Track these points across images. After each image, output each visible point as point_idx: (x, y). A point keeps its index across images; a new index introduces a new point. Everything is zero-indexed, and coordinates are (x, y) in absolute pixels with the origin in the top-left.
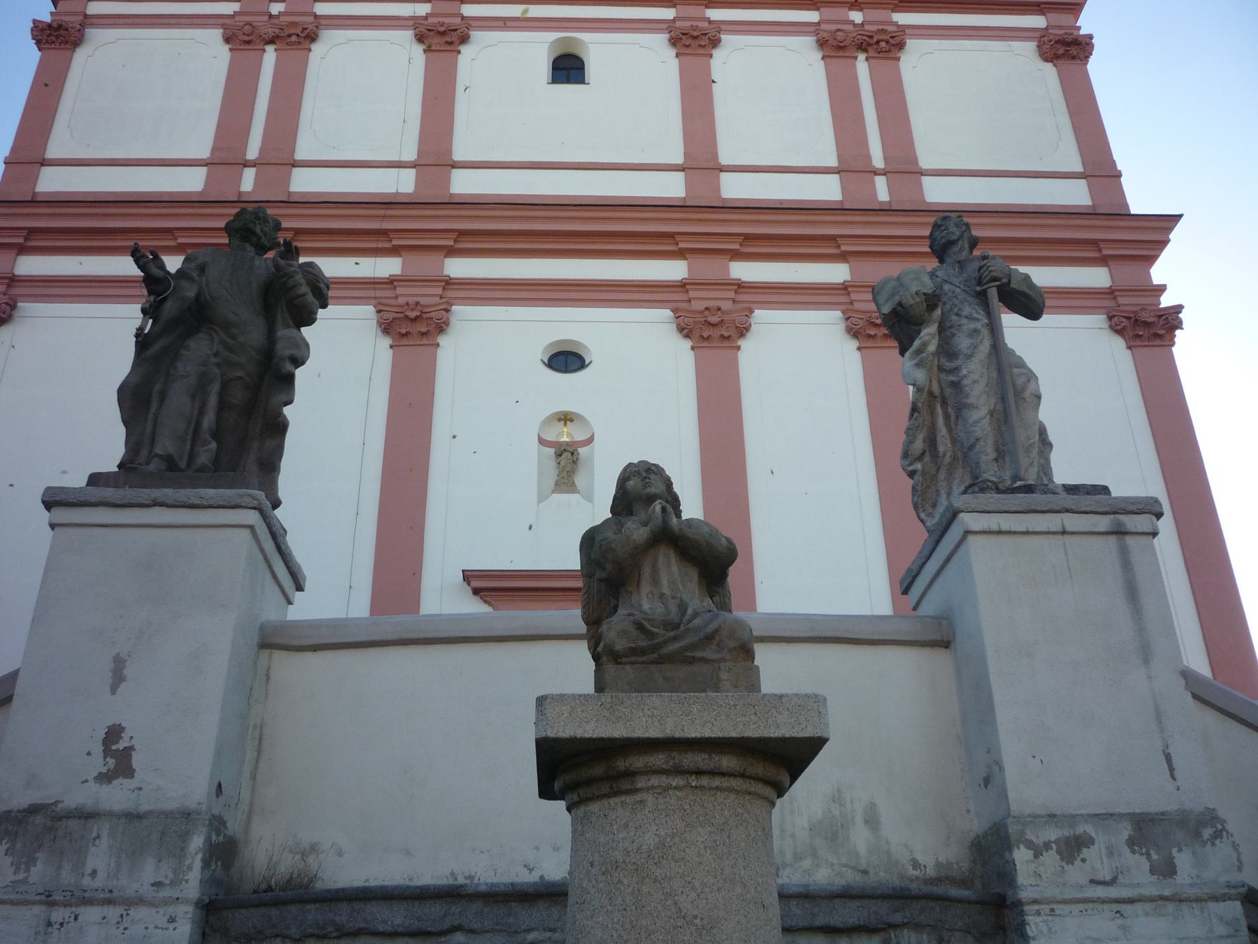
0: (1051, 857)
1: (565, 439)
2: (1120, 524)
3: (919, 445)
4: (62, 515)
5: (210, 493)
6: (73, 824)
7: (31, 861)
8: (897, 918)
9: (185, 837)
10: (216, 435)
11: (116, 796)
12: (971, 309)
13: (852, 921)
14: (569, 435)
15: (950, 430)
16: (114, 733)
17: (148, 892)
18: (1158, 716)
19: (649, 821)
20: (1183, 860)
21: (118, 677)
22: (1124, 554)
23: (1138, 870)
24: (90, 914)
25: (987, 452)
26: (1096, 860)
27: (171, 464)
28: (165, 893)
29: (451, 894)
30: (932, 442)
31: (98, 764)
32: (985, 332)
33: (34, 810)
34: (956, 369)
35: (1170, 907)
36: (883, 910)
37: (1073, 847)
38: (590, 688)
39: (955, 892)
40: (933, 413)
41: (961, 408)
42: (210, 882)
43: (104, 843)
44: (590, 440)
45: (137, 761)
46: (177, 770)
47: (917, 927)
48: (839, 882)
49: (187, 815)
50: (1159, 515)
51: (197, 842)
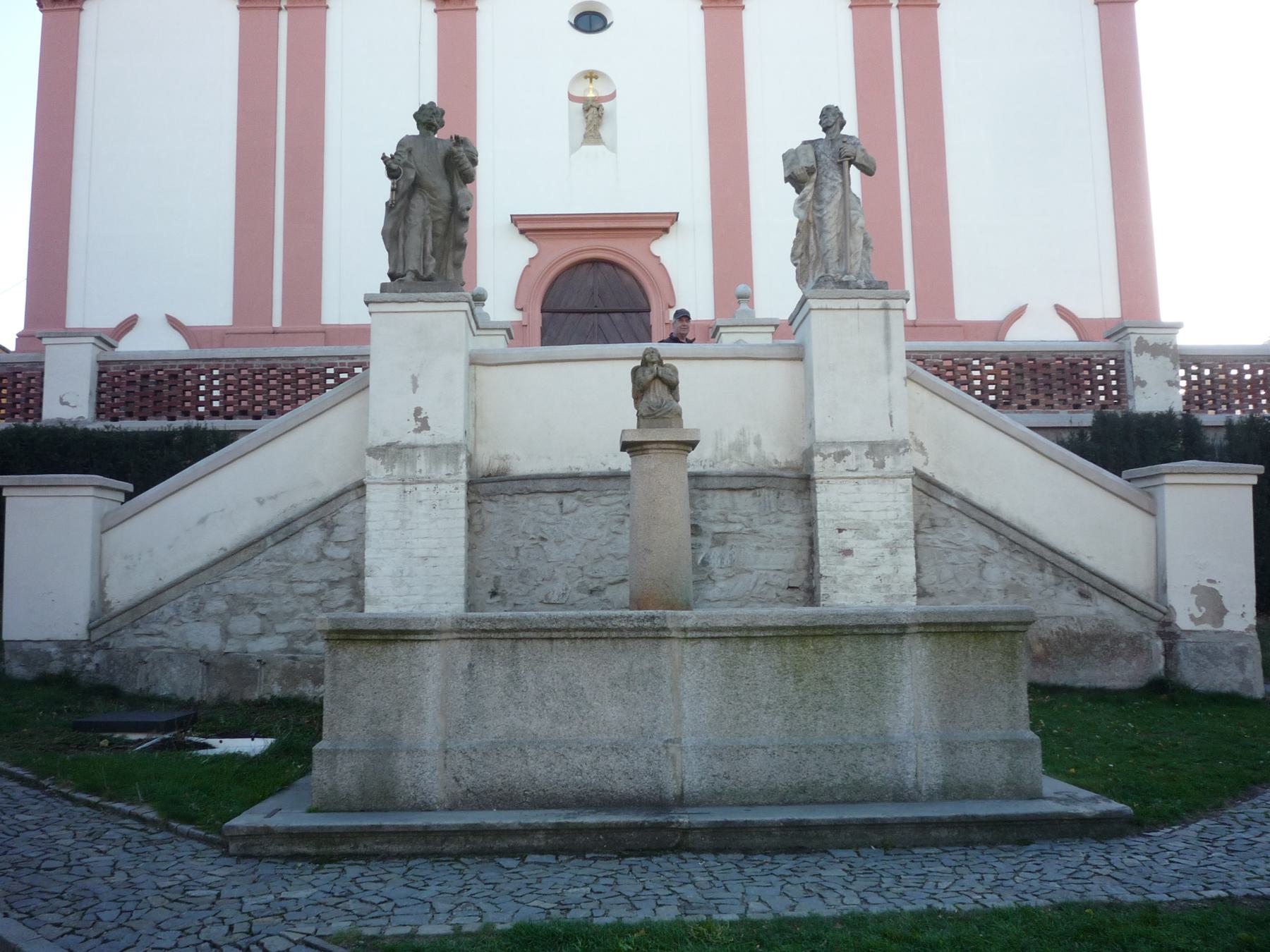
0: (830, 460)
1: (591, 95)
2: (887, 304)
3: (799, 250)
4: (374, 307)
5: (444, 294)
6: (408, 451)
7: (393, 467)
8: (760, 485)
9: (457, 455)
10: (433, 254)
11: (424, 438)
12: (834, 173)
13: (740, 486)
14: (594, 91)
15: (816, 242)
16: (418, 411)
17: (446, 478)
18: (890, 398)
19: (651, 461)
20: (889, 462)
21: (415, 386)
22: (887, 319)
23: (868, 467)
24: (421, 487)
25: (833, 257)
26: (850, 461)
27: (418, 277)
28: (453, 478)
29: (576, 476)
30: (806, 248)
31: (413, 425)
32: (839, 187)
33: (389, 445)
34: (820, 211)
35: (880, 480)
36: (754, 482)
37: (840, 456)
38: (634, 426)
39: (786, 474)
40: (808, 231)
41: (822, 232)
42: (469, 473)
43: (423, 458)
44: (613, 96)
45: (430, 422)
46: (448, 425)
47: (769, 488)
48: (741, 470)
49: (456, 446)
50: (907, 300)
51: (463, 457)
